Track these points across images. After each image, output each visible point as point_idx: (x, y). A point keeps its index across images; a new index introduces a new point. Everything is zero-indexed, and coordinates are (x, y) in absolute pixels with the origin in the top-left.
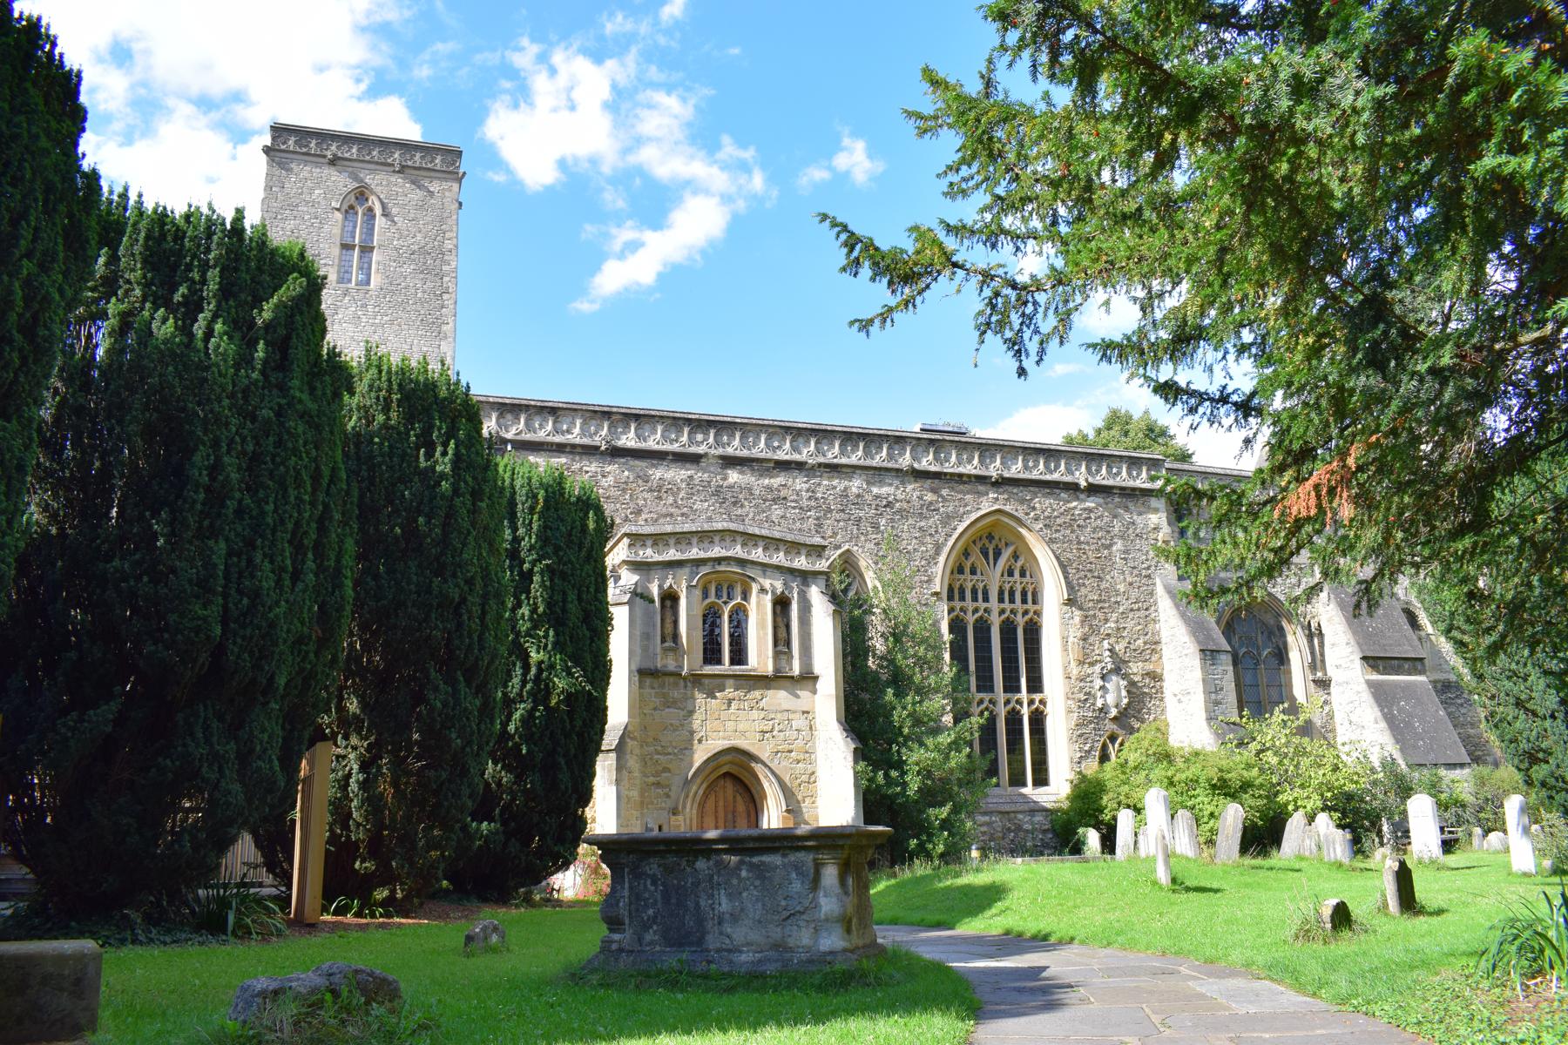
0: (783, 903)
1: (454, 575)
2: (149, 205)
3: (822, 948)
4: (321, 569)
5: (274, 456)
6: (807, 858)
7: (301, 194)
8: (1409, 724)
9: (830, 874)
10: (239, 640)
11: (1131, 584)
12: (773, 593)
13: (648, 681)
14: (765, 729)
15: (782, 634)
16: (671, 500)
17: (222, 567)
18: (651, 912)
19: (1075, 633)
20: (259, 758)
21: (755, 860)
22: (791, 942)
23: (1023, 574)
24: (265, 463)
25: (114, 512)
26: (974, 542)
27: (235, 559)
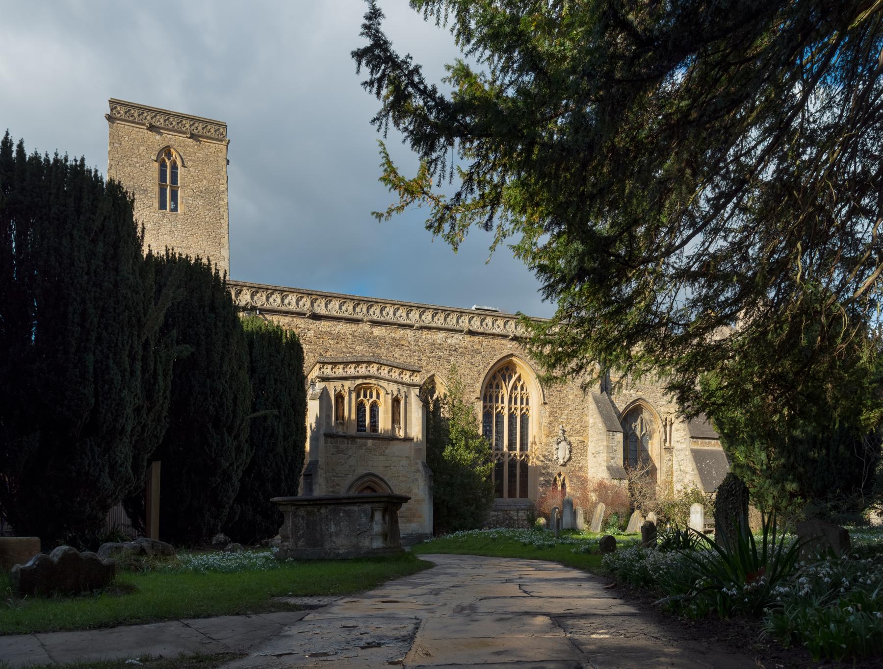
0: (358, 527)
1: (219, 378)
2: (29, 153)
3: (374, 547)
4: (144, 370)
5: (115, 309)
6: (368, 507)
7: (133, 149)
8: (709, 472)
9: (378, 516)
10: (105, 407)
11: (576, 396)
12: (393, 395)
13: (329, 440)
14: (387, 465)
15: (397, 417)
16: (344, 344)
17: (92, 368)
18: (301, 532)
19: (545, 421)
20: (121, 466)
21: (347, 508)
22: (361, 545)
23: (522, 389)
24: (110, 313)
25: (33, 338)
26: (499, 371)
27: (100, 365)
